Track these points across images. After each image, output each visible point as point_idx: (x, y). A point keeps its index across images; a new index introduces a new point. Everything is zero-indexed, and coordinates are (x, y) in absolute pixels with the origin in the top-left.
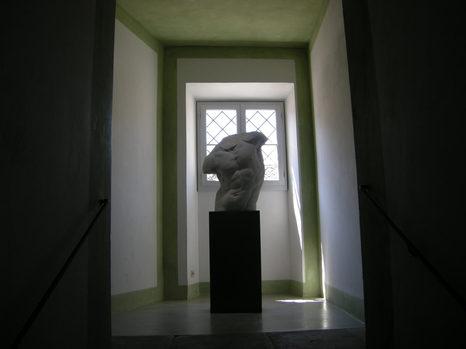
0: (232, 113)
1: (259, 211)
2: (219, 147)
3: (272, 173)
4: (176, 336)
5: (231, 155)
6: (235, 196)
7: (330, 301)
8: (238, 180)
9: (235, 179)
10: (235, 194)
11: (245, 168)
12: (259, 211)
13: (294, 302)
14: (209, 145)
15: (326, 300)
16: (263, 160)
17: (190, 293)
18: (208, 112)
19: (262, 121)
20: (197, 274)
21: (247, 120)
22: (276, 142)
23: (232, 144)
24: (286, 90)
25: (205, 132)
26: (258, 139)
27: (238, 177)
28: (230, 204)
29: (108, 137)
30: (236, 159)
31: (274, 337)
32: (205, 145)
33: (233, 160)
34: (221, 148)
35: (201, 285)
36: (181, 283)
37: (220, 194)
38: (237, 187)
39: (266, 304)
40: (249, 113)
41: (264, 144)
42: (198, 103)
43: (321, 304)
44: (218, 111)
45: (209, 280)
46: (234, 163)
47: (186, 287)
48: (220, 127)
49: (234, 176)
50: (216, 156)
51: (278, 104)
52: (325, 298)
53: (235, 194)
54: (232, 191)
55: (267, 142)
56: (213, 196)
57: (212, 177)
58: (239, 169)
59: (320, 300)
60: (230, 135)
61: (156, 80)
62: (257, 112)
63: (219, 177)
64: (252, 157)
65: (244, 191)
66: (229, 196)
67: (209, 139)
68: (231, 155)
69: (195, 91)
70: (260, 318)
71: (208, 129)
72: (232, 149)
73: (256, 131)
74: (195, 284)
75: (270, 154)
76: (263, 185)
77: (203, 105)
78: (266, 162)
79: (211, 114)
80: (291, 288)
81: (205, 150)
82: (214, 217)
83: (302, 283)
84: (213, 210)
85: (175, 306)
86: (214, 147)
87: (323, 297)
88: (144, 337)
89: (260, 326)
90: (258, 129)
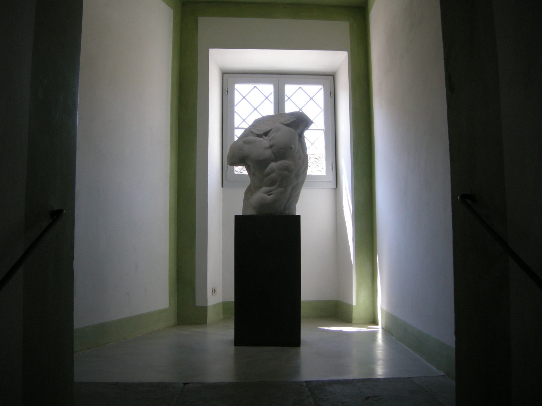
0: (268, 89)
1: (299, 216)
2: (248, 132)
3: (317, 166)
4: (185, 384)
5: (265, 142)
6: (269, 195)
7: (387, 331)
8: (273, 175)
9: (269, 174)
10: (269, 193)
11: (282, 159)
12: (299, 216)
13: (341, 331)
14: (238, 128)
15: (382, 328)
16: (306, 149)
17: (211, 315)
18: (237, 86)
19: (304, 99)
20: (219, 291)
21: (286, 98)
22: (323, 127)
23: (266, 128)
24: (337, 60)
25: (232, 112)
26: (300, 122)
27: (273, 171)
28: (262, 206)
29: (70, 111)
30: (271, 147)
31: (317, 388)
32: (233, 128)
33: (267, 148)
34: (252, 132)
35: (225, 304)
36: (199, 303)
37: (250, 192)
38: (272, 183)
39: (307, 332)
40: (289, 89)
41: (308, 129)
42: (224, 75)
43: (373, 335)
44: (251, 86)
45: (233, 300)
46: (268, 153)
47: (206, 308)
48: (253, 105)
49: (268, 170)
50: (245, 142)
51: (327, 78)
52: (379, 328)
53: (269, 193)
54: (265, 189)
55: (312, 127)
56: (240, 194)
57: (240, 170)
58: (275, 160)
59: (373, 328)
60: (264, 115)
61: (171, 43)
62: (300, 88)
63: (248, 169)
64: (292, 146)
65: (282, 189)
66: (261, 195)
67: (237, 121)
68: (265, 142)
69: (221, 59)
70: (298, 355)
71: (236, 109)
72: (266, 134)
73: (299, 112)
74: (218, 304)
75: (314, 141)
76: (306, 180)
77: (230, 77)
78: (310, 152)
79: (241, 89)
80: (338, 312)
81: (233, 135)
82: (241, 222)
83: (352, 305)
84: (240, 213)
85: (191, 332)
86: (243, 131)
87: (374, 322)
88: (142, 385)
89: (296, 369)
90: (301, 109)
